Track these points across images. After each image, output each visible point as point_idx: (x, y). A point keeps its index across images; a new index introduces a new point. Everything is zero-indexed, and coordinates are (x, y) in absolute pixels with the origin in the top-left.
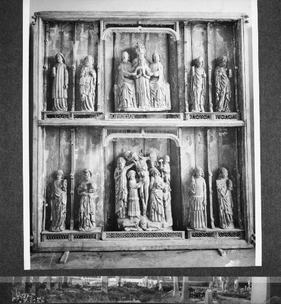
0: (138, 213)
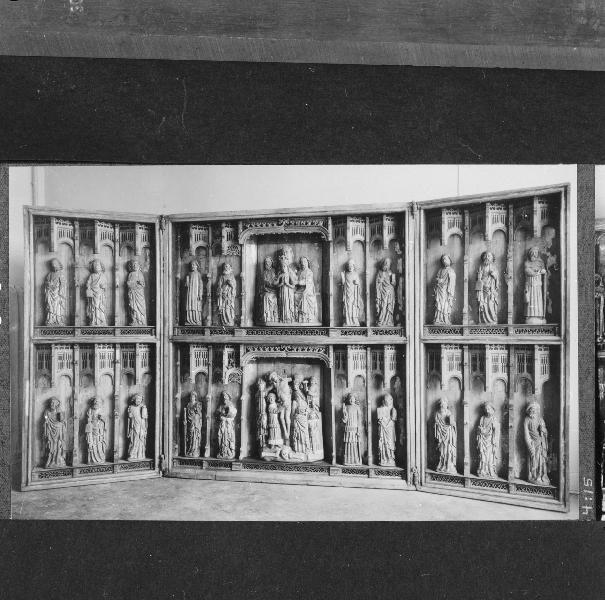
0: (280, 442)
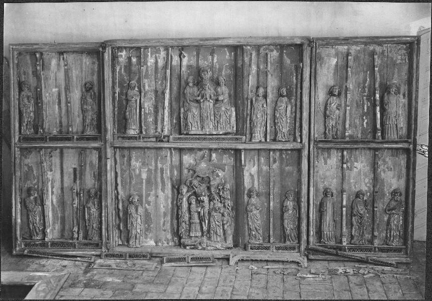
0: (199, 234)
